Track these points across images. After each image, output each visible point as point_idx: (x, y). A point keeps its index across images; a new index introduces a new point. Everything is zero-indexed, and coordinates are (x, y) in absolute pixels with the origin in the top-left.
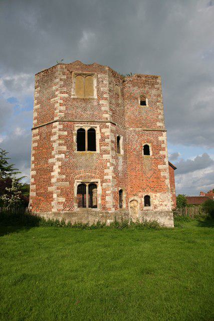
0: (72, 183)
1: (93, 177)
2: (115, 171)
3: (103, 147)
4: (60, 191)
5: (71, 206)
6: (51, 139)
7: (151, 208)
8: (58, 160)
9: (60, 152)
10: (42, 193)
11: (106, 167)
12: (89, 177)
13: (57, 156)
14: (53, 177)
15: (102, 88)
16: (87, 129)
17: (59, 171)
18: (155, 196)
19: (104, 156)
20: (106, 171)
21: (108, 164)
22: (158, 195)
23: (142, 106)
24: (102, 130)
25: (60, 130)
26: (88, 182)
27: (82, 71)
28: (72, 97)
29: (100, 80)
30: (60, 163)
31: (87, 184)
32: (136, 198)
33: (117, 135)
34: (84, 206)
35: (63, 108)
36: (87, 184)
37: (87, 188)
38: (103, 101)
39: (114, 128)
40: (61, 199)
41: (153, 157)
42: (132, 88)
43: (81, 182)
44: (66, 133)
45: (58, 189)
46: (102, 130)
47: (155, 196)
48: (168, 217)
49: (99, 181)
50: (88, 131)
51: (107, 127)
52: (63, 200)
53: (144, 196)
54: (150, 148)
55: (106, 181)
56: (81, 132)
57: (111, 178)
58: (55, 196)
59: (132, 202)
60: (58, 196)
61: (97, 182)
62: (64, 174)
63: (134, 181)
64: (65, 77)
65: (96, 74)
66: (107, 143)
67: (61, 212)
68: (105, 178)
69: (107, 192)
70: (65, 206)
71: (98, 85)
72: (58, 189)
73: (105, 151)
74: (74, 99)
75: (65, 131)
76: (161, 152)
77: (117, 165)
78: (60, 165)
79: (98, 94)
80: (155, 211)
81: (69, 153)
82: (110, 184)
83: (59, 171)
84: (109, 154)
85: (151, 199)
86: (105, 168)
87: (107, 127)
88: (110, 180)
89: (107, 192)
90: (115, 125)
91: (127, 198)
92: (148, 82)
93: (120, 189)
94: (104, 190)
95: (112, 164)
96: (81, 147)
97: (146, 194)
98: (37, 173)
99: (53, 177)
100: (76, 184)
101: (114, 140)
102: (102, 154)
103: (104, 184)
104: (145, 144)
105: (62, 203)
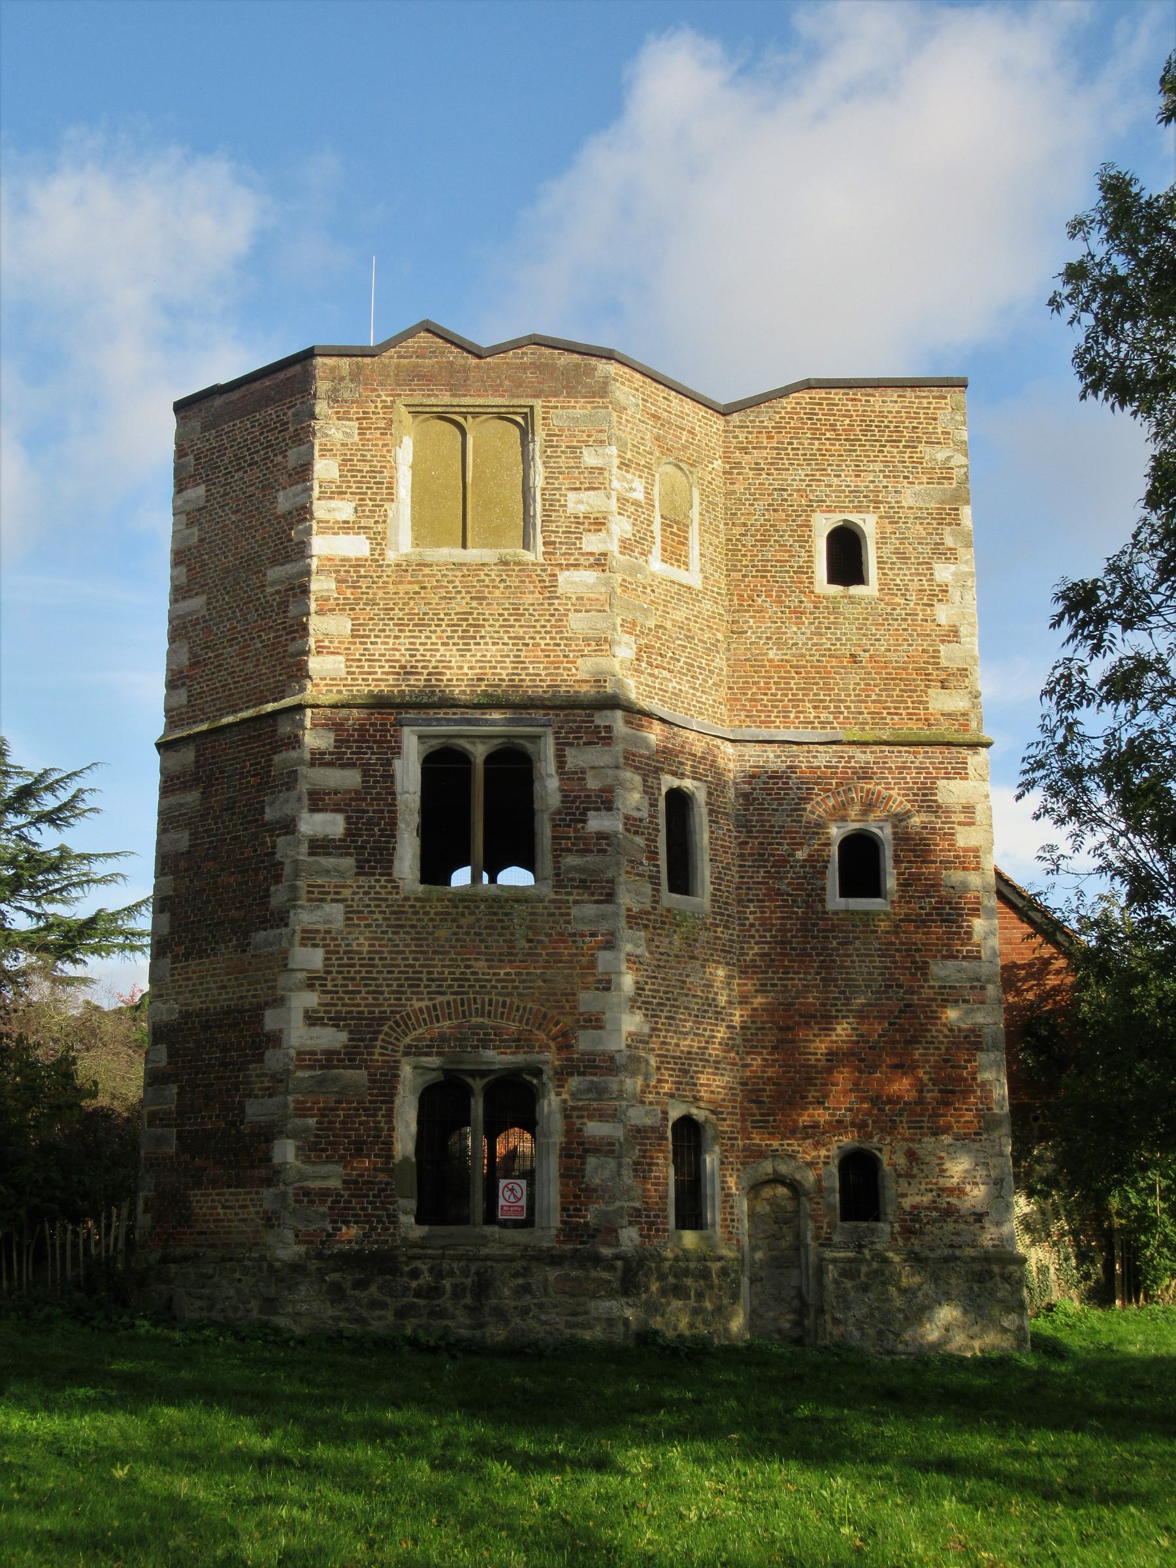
3: (571, 860)
4: (312, 1122)
6: (269, 815)
15: (572, 496)
16: (479, 752)
23: (836, 590)
26: (482, 1074)
31: (478, 1085)
36: (478, 1085)
44: (350, 779)
50: (490, 759)
58: (286, 1152)
61: (538, 1073)
75: (350, 765)
105: (324, 1193)
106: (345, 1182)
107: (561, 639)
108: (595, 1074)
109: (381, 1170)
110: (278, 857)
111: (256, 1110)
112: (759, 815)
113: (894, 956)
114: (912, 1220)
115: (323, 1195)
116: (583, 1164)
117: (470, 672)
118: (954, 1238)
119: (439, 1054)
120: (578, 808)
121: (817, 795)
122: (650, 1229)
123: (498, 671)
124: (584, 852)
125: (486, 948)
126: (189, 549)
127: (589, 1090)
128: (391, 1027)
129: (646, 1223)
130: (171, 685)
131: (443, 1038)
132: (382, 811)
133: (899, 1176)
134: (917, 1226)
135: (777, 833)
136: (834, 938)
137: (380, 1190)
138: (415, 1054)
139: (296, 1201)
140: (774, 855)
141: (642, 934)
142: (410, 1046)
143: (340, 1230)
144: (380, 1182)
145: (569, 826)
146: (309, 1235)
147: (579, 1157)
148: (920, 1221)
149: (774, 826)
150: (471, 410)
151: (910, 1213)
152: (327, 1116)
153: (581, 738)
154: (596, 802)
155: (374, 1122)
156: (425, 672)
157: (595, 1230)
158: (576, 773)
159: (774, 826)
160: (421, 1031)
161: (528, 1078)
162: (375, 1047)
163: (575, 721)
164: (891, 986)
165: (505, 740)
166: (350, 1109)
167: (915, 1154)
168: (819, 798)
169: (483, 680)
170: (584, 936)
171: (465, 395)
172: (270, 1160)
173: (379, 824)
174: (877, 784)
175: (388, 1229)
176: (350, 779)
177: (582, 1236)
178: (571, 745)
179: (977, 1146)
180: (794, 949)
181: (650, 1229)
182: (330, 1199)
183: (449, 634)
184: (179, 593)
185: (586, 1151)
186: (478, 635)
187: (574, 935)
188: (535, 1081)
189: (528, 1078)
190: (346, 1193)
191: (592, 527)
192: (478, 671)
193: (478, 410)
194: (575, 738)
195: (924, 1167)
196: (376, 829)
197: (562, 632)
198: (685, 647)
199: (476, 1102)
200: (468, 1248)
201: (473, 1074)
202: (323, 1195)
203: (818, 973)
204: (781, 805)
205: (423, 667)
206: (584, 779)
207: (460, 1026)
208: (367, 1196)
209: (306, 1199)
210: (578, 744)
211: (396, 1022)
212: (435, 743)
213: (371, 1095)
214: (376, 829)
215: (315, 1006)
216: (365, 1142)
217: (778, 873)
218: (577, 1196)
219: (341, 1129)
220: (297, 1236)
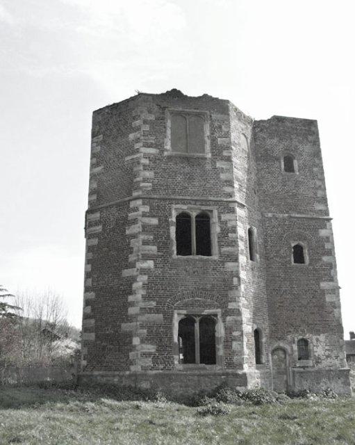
0: (169, 318)
3: (225, 249)
4: (145, 331)
5: (169, 361)
6: (128, 232)
7: (311, 363)
8: (143, 271)
9: (146, 257)
10: (108, 335)
14: (132, 304)
15: (219, 139)
16: (194, 214)
18: (317, 340)
23: (288, 173)
25: (144, 215)
26: (199, 316)
28: (166, 153)
29: (216, 124)
31: (197, 319)
32: (282, 344)
35: (149, 174)
36: (197, 319)
37: (197, 326)
38: (223, 162)
41: (311, 267)
42: (268, 142)
43: (186, 315)
44: (155, 221)
47: (317, 340)
50: (197, 217)
54: (306, 251)
58: (136, 341)
60: (142, 342)
61: (216, 315)
70: (155, 360)
71: (212, 134)
72: (142, 327)
74: (170, 158)
75: (154, 216)
76: (325, 259)
78: (147, 282)
79: (212, 149)
81: (162, 258)
85: (311, 346)
96: (184, 248)
97: (301, 337)
98: (97, 296)
99: (132, 304)
100: (176, 320)
102: (223, 263)
103: (228, 318)
105: (150, 354)
110: (131, 246)
111: (125, 327)
124: (228, 246)
126: (165, 128)
130: (90, 194)
172: (131, 343)
176: (155, 221)
184: (93, 166)
185: (232, 340)
200: (109, 378)
201: (195, 316)
212: (181, 211)
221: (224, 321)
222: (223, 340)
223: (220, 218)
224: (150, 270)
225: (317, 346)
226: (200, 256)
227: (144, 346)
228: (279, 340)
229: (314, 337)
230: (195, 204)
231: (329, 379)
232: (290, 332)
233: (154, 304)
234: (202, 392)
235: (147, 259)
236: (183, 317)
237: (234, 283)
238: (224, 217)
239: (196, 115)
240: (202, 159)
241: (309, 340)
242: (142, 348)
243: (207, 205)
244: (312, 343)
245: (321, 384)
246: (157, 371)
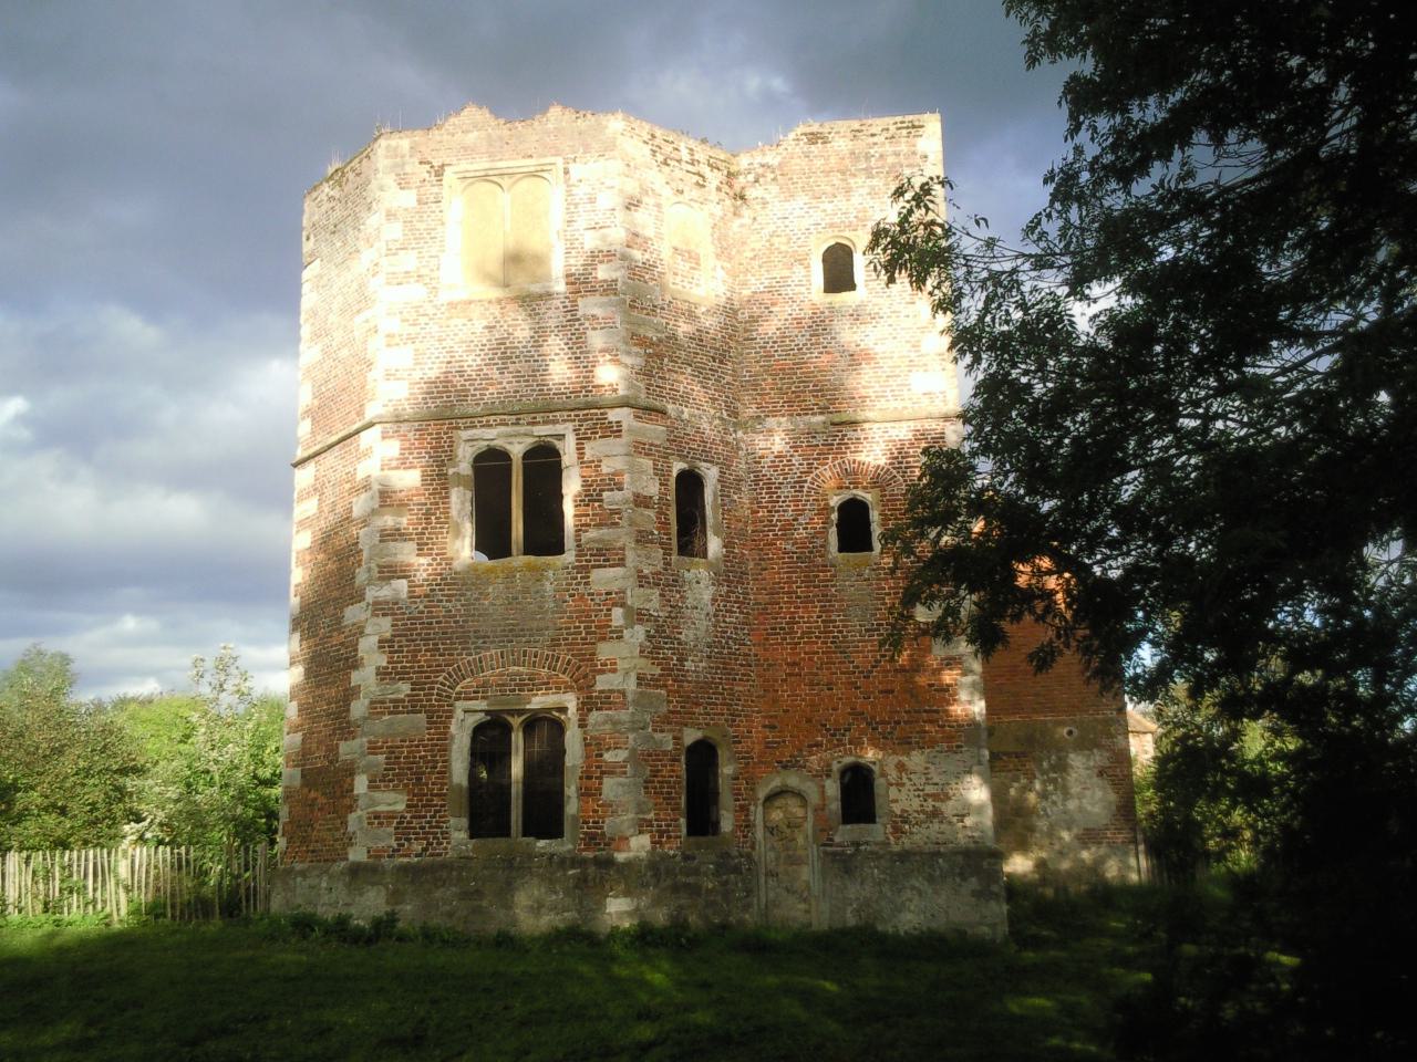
0: (439, 719)
1: (533, 684)
2: (662, 638)
3: (592, 534)
4: (381, 758)
5: (436, 834)
7: (878, 832)
8: (380, 608)
11: (607, 633)
12: (521, 687)
13: (372, 594)
16: (517, 450)
17: (382, 660)
18: (901, 767)
19: (596, 574)
20: (605, 651)
21: (617, 614)
22: (916, 759)
24: (588, 446)
26: (520, 712)
27: (491, 156)
30: (385, 626)
32: (793, 780)
33: (678, 466)
34: (503, 830)
36: (516, 722)
39: (655, 431)
40: (392, 796)
43: (487, 712)
45: (373, 749)
46: (588, 446)
47: (901, 767)
48: (973, 883)
49: (571, 701)
50: (527, 455)
51: (614, 431)
52: (394, 801)
53: (836, 767)
55: (606, 701)
56: (491, 467)
57: (631, 685)
58: (361, 784)
59: (778, 803)
60: (373, 786)
62: (402, 675)
63: (784, 693)
64: (408, 198)
65: (559, 161)
66: (614, 512)
67: (385, 861)
68: (599, 687)
69: (608, 756)
70: (403, 832)
72: (373, 749)
73: (600, 552)
77: (676, 612)
80: (896, 849)
82: (624, 715)
83: (382, 660)
84: (621, 563)
86: (604, 639)
87: (614, 431)
88: (623, 693)
89: (608, 756)
90: (663, 412)
91: (748, 778)
92: (868, 157)
93: (691, 736)
94: (594, 747)
95: (638, 616)
97: (849, 760)
101: (653, 489)
102: (584, 570)
104: (846, 495)
105: (391, 816)
106: (408, 806)
107: (581, 353)
108: (610, 709)
109: (437, 795)
112: (768, 488)
113: (884, 599)
114: (902, 822)
115: (390, 817)
116: (601, 784)
117: (507, 386)
118: (939, 836)
119: (483, 698)
120: (594, 490)
121: (816, 468)
122: (661, 837)
123: (531, 383)
125: (831, 668)
127: (605, 722)
128: (445, 678)
129: (657, 831)
131: (485, 685)
132: (437, 504)
133: (892, 785)
134: (907, 827)
135: (783, 502)
136: (832, 586)
137: (436, 812)
138: (466, 699)
139: (369, 823)
140: (781, 521)
141: (656, 590)
142: (460, 693)
143: (403, 845)
144: (436, 805)
145: (588, 505)
146: (379, 851)
147: (596, 778)
148: (909, 823)
149: (780, 497)
150: (506, 171)
151: (900, 816)
152: (394, 752)
153: (597, 433)
154: (610, 485)
155: (432, 756)
156: (885, 375)
157: (610, 838)
158: (593, 461)
159: (780, 497)
160: (469, 680)
161: (557, 714)
162: (433, 695)
163: (592, 419)
164: (882, 625)
165: (537, 439)
166: (412, 746)
167: (903, 765)
168: (818, 471)
169: (518, 392)
170: (601, 594)
171: (501, 160)
172: (352, 790)
173: (434, 514)
174: (868, 456)
175: (442, 844)
177: (599, 844)
178: (589, 439)
179: (958, 757)
180: (798, 597)
181: (661, 837)
182: (395, 821)
183: (491, 356)
185: (603, 773)
186: (514, 356)
187: (593, 594)
188: (563, 717)
189: (557, 714)
190: (409, 815)
191: (606, 259)
192: (514, 384)
193: (510, 171)
194: (592, 433)
195: (912, 776)
196: (433, 518)
197: (581, 347)
198: (698, 354)
199: (517, 736)
201: (512, 713)
202: (390, 817)
203: (819, 617)
204: (786, 479)
205: (470, 385)
206: (600, 466)
207: (501, 675)
208: (425, 817)
209: (376, 821)
210: (595, 438)
211: (449, 674)
212: (483, 445)
213: (429, 734)
214: (433, 518)
215: (385, 664)
216: (424, 773)
217: (785, 535)
218: (595, 811)
219: (404, 763)
220: (369, 852)
221: (582, 724)
222: (579, 773)
223: (581, 454)
224: (397, 603)
225: (900, 785)
226: (532, 558)
227: (377, 795)
228: (785, 767)
229: (893, 760)
230: (517, 424)
231: (931, 879)
232: (818, 745)
233: (405, 688)
234: (626, 947)
235: (393, 577)
236: (480, 717)
237: (614, 624)
238: (590, 450)
239: (533, 175)
240: (541, 297)
241: (876, 769)
242: (374, 803)
243: (546, 423)
244: (884, 775)
245: (908, 894)
246: (406, 860)
